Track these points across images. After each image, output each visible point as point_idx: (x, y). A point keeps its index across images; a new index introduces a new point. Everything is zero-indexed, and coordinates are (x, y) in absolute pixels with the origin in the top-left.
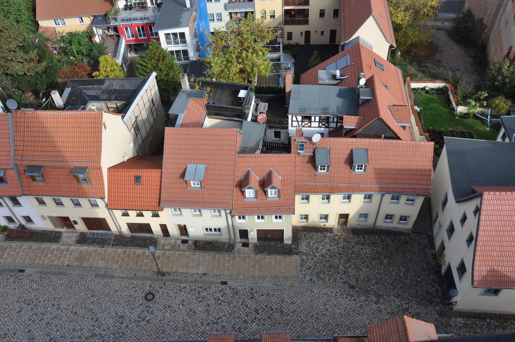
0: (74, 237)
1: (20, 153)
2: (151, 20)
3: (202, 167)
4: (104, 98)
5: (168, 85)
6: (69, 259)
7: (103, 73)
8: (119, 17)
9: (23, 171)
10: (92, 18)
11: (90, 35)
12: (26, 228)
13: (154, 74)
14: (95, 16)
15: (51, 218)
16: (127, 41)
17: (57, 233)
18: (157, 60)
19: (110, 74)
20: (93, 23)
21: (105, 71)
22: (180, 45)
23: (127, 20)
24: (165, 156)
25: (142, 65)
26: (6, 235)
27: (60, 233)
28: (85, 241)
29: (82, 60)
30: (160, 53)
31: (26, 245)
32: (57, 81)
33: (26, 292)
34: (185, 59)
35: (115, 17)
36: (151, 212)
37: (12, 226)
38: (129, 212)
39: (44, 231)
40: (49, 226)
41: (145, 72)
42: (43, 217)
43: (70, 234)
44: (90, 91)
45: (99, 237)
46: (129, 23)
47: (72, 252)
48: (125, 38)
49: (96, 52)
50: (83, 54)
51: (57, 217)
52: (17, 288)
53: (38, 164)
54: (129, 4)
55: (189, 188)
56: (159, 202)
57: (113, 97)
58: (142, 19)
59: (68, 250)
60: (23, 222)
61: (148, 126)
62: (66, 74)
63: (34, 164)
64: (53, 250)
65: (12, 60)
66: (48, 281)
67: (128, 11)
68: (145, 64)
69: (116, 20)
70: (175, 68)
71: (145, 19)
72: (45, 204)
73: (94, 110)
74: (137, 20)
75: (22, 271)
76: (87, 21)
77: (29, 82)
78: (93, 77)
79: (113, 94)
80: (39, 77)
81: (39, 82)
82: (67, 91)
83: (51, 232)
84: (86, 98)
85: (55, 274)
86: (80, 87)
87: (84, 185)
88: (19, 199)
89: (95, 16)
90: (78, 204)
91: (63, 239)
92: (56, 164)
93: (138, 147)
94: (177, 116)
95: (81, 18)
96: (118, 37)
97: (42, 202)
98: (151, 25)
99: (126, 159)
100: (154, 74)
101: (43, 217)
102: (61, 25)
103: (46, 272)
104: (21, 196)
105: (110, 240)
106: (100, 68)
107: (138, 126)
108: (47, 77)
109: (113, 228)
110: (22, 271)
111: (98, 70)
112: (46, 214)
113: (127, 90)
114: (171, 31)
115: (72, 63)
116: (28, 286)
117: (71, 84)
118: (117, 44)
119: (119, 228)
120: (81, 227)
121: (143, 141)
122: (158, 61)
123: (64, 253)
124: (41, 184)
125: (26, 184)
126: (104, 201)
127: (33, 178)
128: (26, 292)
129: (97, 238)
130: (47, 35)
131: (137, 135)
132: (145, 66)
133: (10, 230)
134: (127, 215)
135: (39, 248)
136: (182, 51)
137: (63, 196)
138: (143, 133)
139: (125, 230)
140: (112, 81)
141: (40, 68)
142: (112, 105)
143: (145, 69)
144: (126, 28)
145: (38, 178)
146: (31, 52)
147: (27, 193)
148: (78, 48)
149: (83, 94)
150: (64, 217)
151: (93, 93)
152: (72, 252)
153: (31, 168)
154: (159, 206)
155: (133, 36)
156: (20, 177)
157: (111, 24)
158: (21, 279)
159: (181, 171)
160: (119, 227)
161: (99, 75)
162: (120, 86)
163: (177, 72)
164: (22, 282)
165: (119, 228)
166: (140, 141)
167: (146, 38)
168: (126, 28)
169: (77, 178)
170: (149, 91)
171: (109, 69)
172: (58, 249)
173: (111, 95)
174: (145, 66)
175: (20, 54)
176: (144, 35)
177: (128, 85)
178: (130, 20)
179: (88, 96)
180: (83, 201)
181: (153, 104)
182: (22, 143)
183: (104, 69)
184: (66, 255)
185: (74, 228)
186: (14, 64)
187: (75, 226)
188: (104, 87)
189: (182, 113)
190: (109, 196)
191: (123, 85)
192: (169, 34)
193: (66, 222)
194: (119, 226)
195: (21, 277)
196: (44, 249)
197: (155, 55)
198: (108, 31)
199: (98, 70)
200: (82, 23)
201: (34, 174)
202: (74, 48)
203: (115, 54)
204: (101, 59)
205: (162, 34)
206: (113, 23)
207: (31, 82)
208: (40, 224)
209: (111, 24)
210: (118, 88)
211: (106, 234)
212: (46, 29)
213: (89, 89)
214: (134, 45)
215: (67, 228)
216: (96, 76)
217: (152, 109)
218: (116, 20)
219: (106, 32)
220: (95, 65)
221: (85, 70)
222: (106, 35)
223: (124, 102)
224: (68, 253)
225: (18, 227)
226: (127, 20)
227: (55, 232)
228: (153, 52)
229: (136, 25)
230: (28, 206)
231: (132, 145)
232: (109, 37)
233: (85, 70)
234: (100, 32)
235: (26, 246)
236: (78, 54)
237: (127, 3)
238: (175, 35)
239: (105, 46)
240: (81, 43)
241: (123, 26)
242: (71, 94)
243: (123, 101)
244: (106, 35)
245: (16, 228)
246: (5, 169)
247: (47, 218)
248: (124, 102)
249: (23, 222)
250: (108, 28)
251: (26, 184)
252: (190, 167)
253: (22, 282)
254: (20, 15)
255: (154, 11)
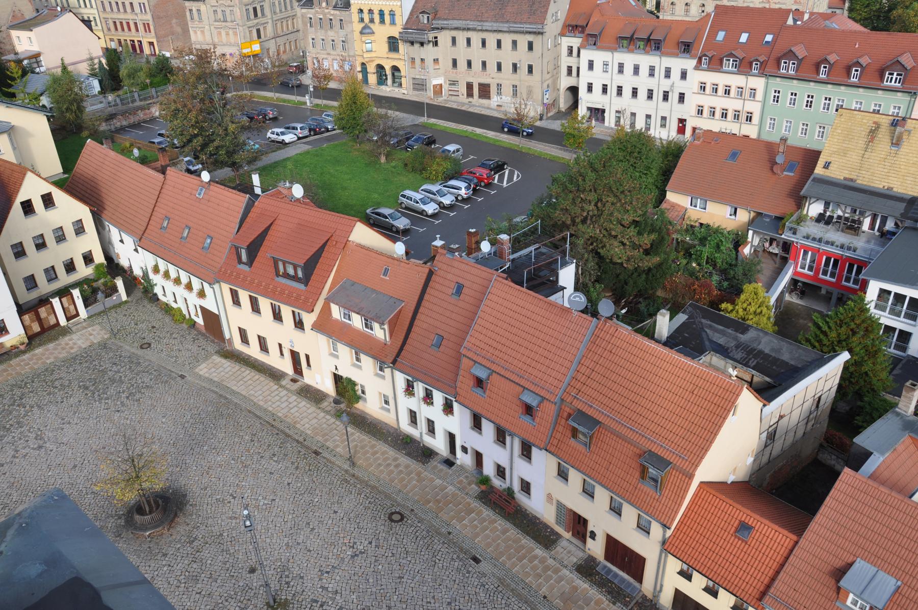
0: (576, 556)
1: (578, 386)
2: (860, 255)
3: (888, 583)
4: (736, 357)
5: (850, 382)
6: (552, 588)
7: (741, 311)
8: (803, 230)
9: (565, 415)
10: (753, 214)
11: (738, 241)
12: (514, 498)
13: (845, 356)
14: (759, 214)
15: (560, 506)
16: (796, 273)
17: (553, 532)
18: (852, 330)
19: (751, 317)
20: (751, 223)
21: (745, 310)
22: (901, 319)
23: (814, 239)
24: (818, 517)
25: (819, 328)
26: (482, 492)
27: (559, 536)
28: (590, 575)
29: (711, 274)
30: (863, 321)
31: (501, 523)
32: (654, 293)
33: (467, 598)
34: (897, 347)
35: (795, 226)
36: (734, 598)
37: (497, 482)
38: (722, 592)
39: (536, 518)
40: (547, 514)
41: (820, 341)
42: (549, 497)
43: (573, 549)
44: (716, 334)
45: (616, 581)
46: (815, 245)
47: (561, 579)
48: (796, 267)
49: (740, 270)
50: (714, 266)
51: (571, 510)
52: (457, 582)
53: (596, 415)
54: (828, 214)
55: (838, 604)
56: (763, 594)
57: (753, 362)
58: (842, 247)
59: (556, 571)
60: (516, 487)
61: (790, 439)
62: (677, 286)
63: (590, 412)
64: (536, 557)
65: (615, 237)
66: (503, 602)
67: (821, 225)
68: (825, 328)
69: (795, 233)
70: (880, 358)
71: (849, 249)
72: (567, 480)
73: (731, 376)
74: (832, 245)
75: (476, 560)
76: (744, 216)
77: (618, 276)
78: (720, 310)
79: (755, 357)
80: (636, 274)
81: (631, 282)
82: (682, 318)
83: (546, 526)
84: (707, 343)
85: (520, 597)
86: (703, 321)
87: (647, 488)
88: (535, 451)
89: (759, 214)
90: (616, 510)
91: (558, 548)
92: (624, 431)
93: (756, 468)
94: (868, 454)
95: (736, 210)
96: (785, 260)
97: (563, 475)
98: (862, 264)
99: (731, 479)
100: (845, 356)
101: (549, 497)
102: (698, 208)
103: (508, 585)
104: (541, 449)
105: (632, 598)
106: (737, 301)
107: (775, 432)
108: (647, 280)
109: (648, 585)
110: (476, 560)
111: (733, 302)
112: (556, 496)
113: (783, 361)
114: (895, 289)
115: (692, 273)
116: (474, 589)
117: (690, 309)
118: (778, 272)
119: (658, 588)
120: (596, 548)
121: (769, 461)
122: (854, 333)
123: (549, 572)
124: (581, 448)
125: (558, 436)
126: (665, 532)
127: (574, 433)
128: (467, 598)
129: (611, 582)
130: (671, 215)
131: (766, 446)
132: (825, 334)
133: (492, 487)
134: (689, 577)
135: (517, 541)
136: (901, 331)
137: (600, 484)
138: (778, 447)
139: (666, 599)
140: (761, 334)
141: (646, 264)
142: (758, 378)
143: (822, 336)
144: (806, 253)
145: (581, 436)
146: (645, 235)
147: (553, 449)
148: (712, 254)
149: (704, 334)
150: (580, 516)
151: (722, 341)
152: (561, 579)
153: (582, 417)
154: (760, 599)
155: (810, 269)
156: (557, 420)
157: (783, 236)
158: (468, 572)
159: (839, 564)
160: (658, 590)
161: (732, 311)
162: (773, 350)
163: (878, 367)
164: (468, 578)
165: (658, 588)
166: (765, 459)
167: (833, 280)
168: (806, 253)
169: (643, 471)
170: (822, 382)
171: (752, 309)
172: (543, 560)
173: (749, 357)
174: (825, 334)
175: (632, 232)
176: (832, 275)
177: (787, 352)
178: (820, 240)
179: (711, 341)
180: (575, 477)
181: (817, 406)
182: (588, 372)
183: (745, 305)
184: (551, 577)
185: (585, 542)
186: (616, 243)
187: (589, 540)
188: (743, 338)
189: (882, 453)
190: (677, 529)
191: (778, 351)
192: (889, 293)
193: (579, 526)
194: (662, 586)
195: (470, 569)
196: (523, 547)
197: (853, 320)
198: (771, 244)
199: (733, 302)
200: (733, 217)
201: (580, 428)
202: (706, 251)
203: (769, 286)
204: (748, 288)
205: (874, 288)
206: (786, 236)
207: (621, 277)
208: (538, 505)
209: (783, 236)
210: (767, 351)
211: (630, 584)
212: (674, 206)
213: (716, 331)
214: (804, 283)
215: (573, 535)
216: (726, 310)
217: (810, 414)
218: (795, 233)
219: (767, 245)
220: (733, 292)
221: (709, 293)
222: (764, 250)
223: (768, 379)
224: (555, 577)
225: (504, 490)
226: (814, 239)
227: (552, 529)
228: (852, 313)
229: (825, 252)
230: (539, 470)
231: (750, 460)
232: (766, 255)
233: (709, 293)
234: (756, 241)
235: (500, 525)
236: (707, 263)
237: (825, 211)
238: (899, 298)
239: (758, 267)
240: (722, 248)
241: (803, 246)
242: (684, 325)
243: (772, 382)
244: (764, 250)
245: (501, 489)
246: (543, 398)
247: (554, 502)
248: (768, 379)
249: (516, 487)
250: (772, 241)
251: (558, 436)
252: (862, 568)
253: (468, 578)
254: (646, 174)
255: (868, 242)
